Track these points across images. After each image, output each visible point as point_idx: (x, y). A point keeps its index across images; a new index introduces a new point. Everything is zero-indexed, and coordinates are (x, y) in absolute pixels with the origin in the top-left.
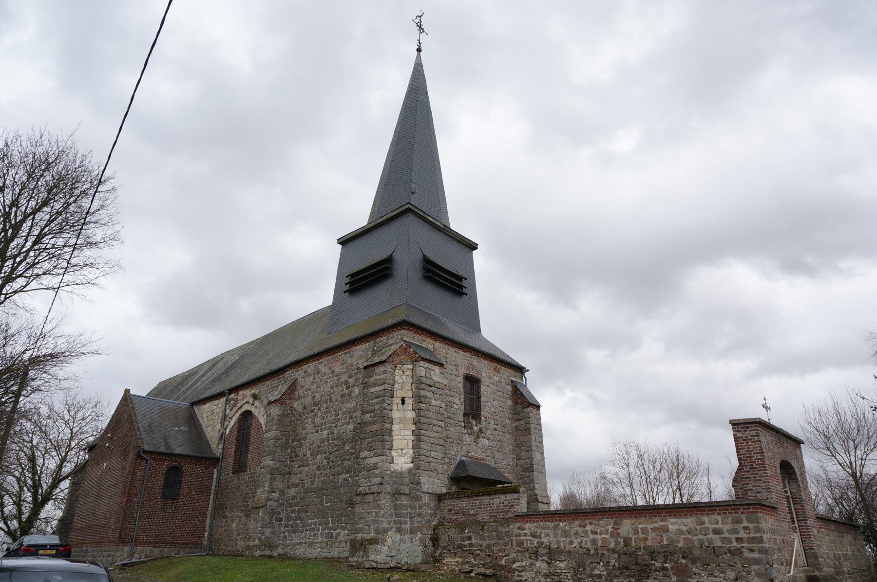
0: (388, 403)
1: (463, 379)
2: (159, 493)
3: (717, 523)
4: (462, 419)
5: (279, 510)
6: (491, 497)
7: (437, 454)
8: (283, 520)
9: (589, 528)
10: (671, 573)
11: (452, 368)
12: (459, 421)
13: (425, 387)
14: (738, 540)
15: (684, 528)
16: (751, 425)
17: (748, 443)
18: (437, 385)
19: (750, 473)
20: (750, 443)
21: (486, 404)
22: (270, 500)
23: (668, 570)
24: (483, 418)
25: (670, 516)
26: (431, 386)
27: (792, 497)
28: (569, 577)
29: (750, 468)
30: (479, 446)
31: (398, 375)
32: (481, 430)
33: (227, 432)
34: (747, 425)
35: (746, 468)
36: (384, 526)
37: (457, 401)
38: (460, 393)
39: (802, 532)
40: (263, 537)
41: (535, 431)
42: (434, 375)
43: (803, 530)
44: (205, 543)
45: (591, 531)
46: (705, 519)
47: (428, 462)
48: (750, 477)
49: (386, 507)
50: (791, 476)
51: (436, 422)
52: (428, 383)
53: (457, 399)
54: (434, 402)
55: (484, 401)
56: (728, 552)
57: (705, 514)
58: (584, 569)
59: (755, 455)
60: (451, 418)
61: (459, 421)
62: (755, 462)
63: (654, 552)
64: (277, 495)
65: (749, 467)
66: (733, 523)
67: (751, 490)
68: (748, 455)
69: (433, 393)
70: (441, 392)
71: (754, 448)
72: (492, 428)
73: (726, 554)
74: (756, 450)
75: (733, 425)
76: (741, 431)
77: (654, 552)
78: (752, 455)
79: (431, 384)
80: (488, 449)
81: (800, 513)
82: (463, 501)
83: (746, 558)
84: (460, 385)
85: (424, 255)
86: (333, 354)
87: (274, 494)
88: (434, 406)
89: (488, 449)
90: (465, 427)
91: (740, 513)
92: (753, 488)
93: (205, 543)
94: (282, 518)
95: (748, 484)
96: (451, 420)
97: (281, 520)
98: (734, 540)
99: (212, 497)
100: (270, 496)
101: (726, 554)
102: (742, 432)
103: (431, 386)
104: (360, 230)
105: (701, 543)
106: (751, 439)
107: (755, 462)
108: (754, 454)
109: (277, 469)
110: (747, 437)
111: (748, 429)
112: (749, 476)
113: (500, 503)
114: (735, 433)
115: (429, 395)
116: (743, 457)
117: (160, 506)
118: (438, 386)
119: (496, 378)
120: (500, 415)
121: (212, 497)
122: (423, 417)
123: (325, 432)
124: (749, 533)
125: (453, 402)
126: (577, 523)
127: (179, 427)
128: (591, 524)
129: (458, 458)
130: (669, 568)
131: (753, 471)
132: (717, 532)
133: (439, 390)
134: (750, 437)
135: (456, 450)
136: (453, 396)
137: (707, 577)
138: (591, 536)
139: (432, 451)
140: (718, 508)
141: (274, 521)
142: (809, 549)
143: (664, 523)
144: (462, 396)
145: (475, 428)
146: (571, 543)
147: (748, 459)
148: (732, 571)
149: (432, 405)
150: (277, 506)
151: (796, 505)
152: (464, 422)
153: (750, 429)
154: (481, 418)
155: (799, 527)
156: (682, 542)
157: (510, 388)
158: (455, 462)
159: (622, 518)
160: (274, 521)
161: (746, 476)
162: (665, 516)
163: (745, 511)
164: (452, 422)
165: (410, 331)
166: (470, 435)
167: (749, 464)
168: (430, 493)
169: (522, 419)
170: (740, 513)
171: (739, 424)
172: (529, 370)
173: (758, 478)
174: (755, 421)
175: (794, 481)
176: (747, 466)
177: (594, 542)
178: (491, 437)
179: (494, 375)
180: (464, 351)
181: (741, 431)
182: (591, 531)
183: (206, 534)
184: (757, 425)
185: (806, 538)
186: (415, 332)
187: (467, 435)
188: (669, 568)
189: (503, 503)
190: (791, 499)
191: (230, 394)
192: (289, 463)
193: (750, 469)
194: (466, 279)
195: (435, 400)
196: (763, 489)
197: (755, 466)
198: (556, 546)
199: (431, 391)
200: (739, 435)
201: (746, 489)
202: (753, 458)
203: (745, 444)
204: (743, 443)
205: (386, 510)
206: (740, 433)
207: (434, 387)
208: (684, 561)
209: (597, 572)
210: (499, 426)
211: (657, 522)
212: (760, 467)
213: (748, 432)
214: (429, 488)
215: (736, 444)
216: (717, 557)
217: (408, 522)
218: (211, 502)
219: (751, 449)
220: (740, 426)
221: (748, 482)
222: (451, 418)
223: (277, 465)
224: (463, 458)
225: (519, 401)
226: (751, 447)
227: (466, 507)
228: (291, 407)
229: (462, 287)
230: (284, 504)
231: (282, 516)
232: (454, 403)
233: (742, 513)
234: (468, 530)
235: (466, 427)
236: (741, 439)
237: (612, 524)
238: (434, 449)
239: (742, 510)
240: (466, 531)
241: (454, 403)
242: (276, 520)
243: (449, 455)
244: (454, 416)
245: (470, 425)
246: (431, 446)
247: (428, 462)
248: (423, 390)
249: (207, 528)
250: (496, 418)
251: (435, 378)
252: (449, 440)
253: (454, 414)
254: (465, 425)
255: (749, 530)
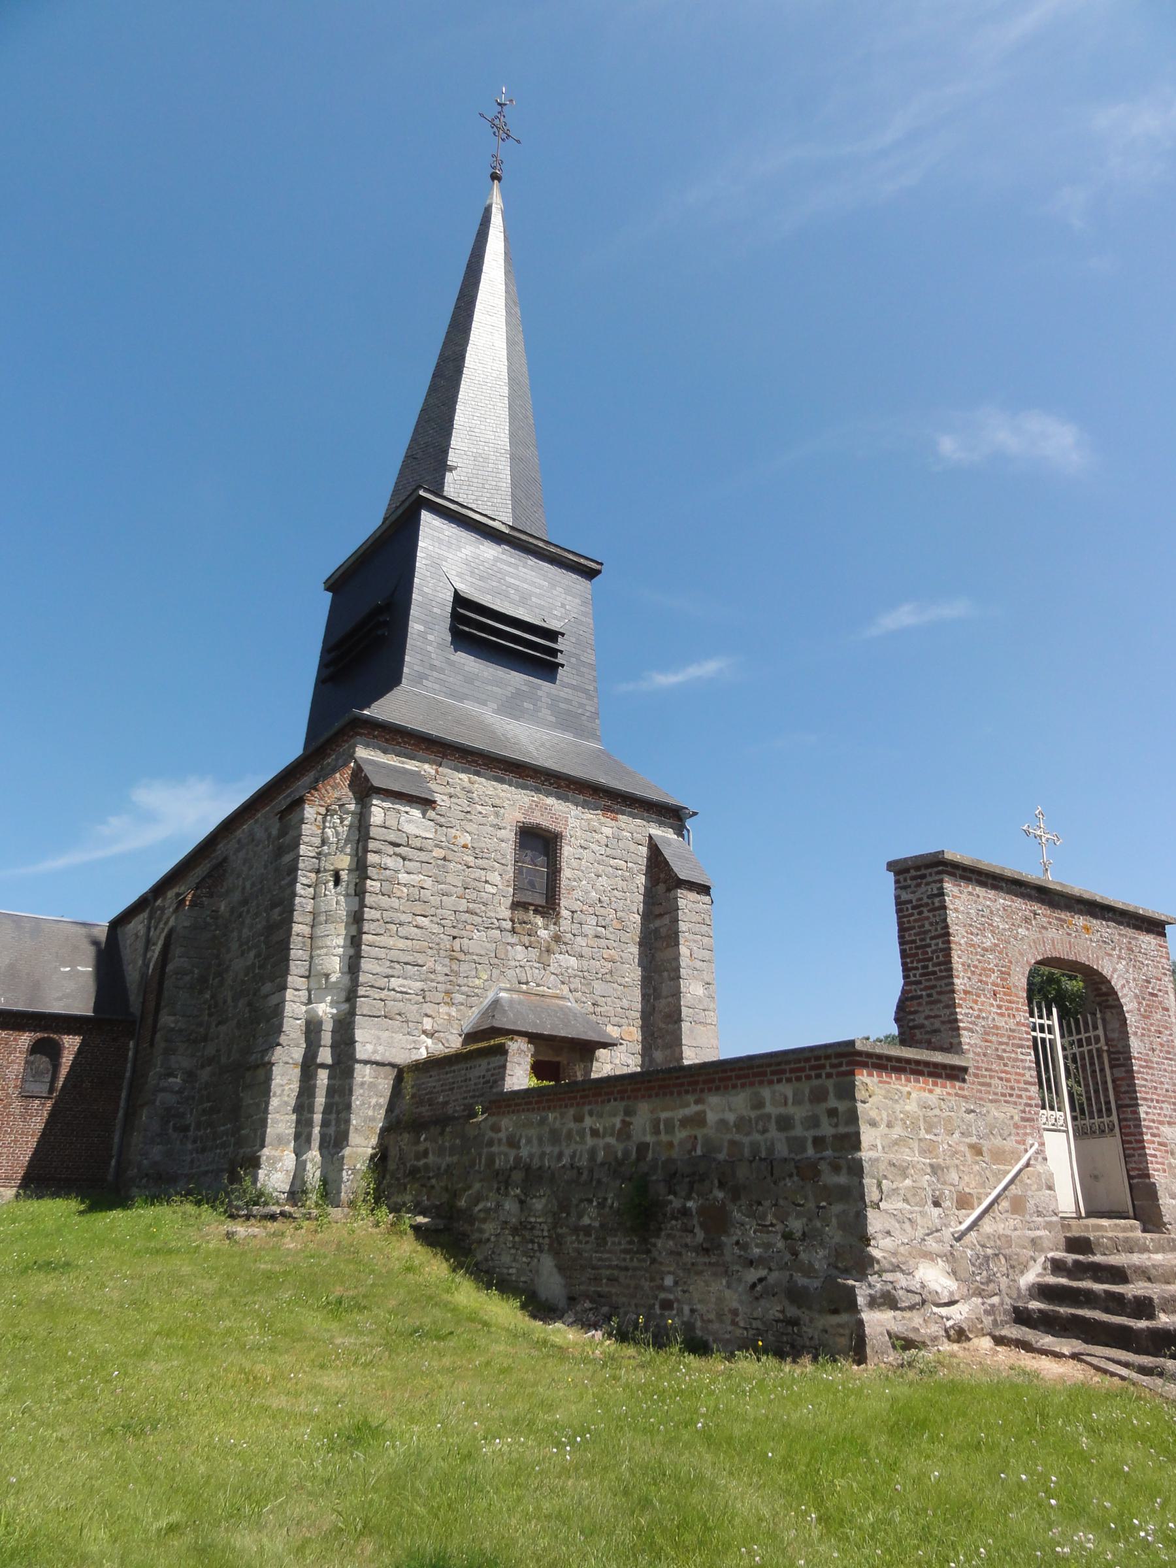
0: (305, 882)
1: (513, 834)
2: (16, 1086)
3: (786, 1104)
4: (507, 914)
5: (181, 1110)
6: (468, 1066)
7: (405, 982)
8: (192, 1128)
9: (588, 1122)
10: (695, 1222)
11: (484, 812)
12: (498, 920)
13: (381, 847)
14: (818, 1142)
15: (731, 1118)
16: (929, 871)
17: (920, 913)
18: (417, 843)
19: (922, 986)
20: (926, 914)
21: (575, 883)
22: (163, 1090)
23: (691, 1215)
24: (565, 913)
25: (710, 1090)
26: (398, 845)
27: (1108, 1051)
28: (546, 1234)
29: (922, 975)
30: (552, 969)
31: (330, 828)
32: (557, 939)
33: (150, 971)
34: (923, 872)
35: (915, 976)
36: (279, 1130)
37: (494, 877)
38: (503, 862)
39: (1127, 1135)
40: (145, 1161)
41: (691, 937)
42: (409, 822)
43: (1127, 1131)
44: (110, 1178)
45: (591, 1129)
46: (766, 1093)
47: (381, 1000)
48: (921, 997)
49: (286, 1093)
50: (1107, 1001)
51: (404, 918)
52: (392, 837)
53: (496, 873)
54: (403, 877)
55: (569, 876)
56: (795, 1172)
57: (766, 1083)
58: (568, 1214)
59: (933, 942)
60: (476, 914)
61: (498, 920)
62: (931, 959)
63: (675, 1173)
64: (178, 1080)
65: (921, 971)
66: (811, 1101)
67: (922, 1026)
68: (919, 943)
69: (404, 859)
70: (423, 856)
71: (931, 924)
72: (591, 933)
73: (791, 1176)
74: (936, 930)
75: (897, 874)
76: (909, 886)
77: (675, 1173)
78: (928, 941)
79: (399, 841)
80: (575, 976)
81: (1123, 1089)
82: (431, 1076)
83: (825, 1186)
84: (503, 844)
85: (456, 591)
86: (271, 801)
87: (171, 1080)
88: (405, 885)
89: (575, 976)
90: (513, 931)
91: (824, 1076)
92: (926, 1022)
93: (110, 1178)
94: (190, 1125)
95: (916, 1012)
96: (475, 917)
97: (186, 1129)
98: (810, 1142)
99: (124, 1095)
100: (163, 1084)
101: (791, 1176)
102: (913, 889)
103: (398, 845)
104: (354, 558)
105: (755, 1148)
106: (927, 904)
107: (931, 959)
108: (932, 938)
109: (181, 1031)
110: (921, 899)
111: (924, 881)
112: (919, 993)
113: (479, 1077)
114: (899, 891)
115: (389, 862)
116: (911, 949)
117: (18, 1111)
118: (419, 845)
119: (608, 831)
120: (614, 906)
121: (124, 1095)
122: (371, 908)
123: (252, 954)
124: (836, 1126)
125: (484, 879)
126: (571, 1112)
127: (73, 967)
128: (591, 1114)
129: (491, 996)
130: (694, 1211)
131: (926, 980)
132: (785, 1123)
133: (419, 853)
134: (926, 900)
135: (485, 977)
136: (484, 869)
137: (754, 1232)
138: (590, 1141)
139: (393, 976)
140: (787, 1067)
141: (170, 1131)
142: (1139, 1176)
143: (699, 1107)
144: (510, 869)
145: (543, 933)
146: (560, 1156)
147: (920, 952)
148: (799, 1216)
149: (398, 884)
150: (178, 1103)
151: (1115, 1070)
152: (512, 920)
153: (929, 879)
154: (559, 913)
155: (1120, 1120)
156: (725, 1151)
157: (644, 850)
158: (481, 1002)
159: (636, 1098)
160: (170, 1131)
161: (914, 994)
162: (702, 1091)
163: (834, 1071)
164: (477, 920)
165: (375, 737)
166: (527, 948)
167: (919, 965)
168: (377, 1063)
169: (665, 914)
170: (824, 1076)
171: (907, 871)
172: (695, 814)
173: (935, 996)
174: (936, 860)
175: (1114, 1011)
176: (916, 968)
177: (593, 1153)
178: (586, 951)
179: (601, 824)
180: (521, 777)
181: (909, 886)
182: (591, 1129)
183: (113, 1163)
184: (941, 868)
185: (1134, 1149)
186: (387, 741)
187: (519, 948)
188: (694, 1211)
189: (484, 1077)
190: (1105, 1055)
191: (155, 900)
192: (206, 1018)
193: (922, 975)
194: (563, 635)
195: (408, 873)
196: (943, 1023)
197: (931, 969)
198: (539, 1164)
199: (399, 855)
200: (905, 896)
201: (911, 1024)
202: (929, 950)
203: (917, 917)
204: (912, 915)
205: (286, 1099)
206: (909, 890)
207: (408, 845)
208: (720, 1195)
209: (586, 1221)
210: (611, 929)
211: (688, 1105)
212: (941, 971)
213: (923, 888)
214: (375, 1052)
215: (899, 918)
216: (775, 1183)
217: (333, 1123)
218: (122, 1104)
219: (927, 927)
220: (908, 876)
221: (916, 1008)
222: (476, 914)
223: (179, 1024)
224: (503, 994)
225: (662, 876)
226: (926, 923)
227: (434, 1087)
228: (213, 911)
229: (554, 652)
230: (193, 1098)
231: (188, 1122)
232: (486, 882)
233: (829, 1076)
234: (424, 1136)
235: (516, 930)
236: (909, 906)
237: (622, 1113)
238: (396, 973)
239: (828, 1070)
240: (422, 1139)
241: (486, 882)
242: (175, 1129)
243: (464, 989)
244: (483, 908)
245: (529, 926)
246: (390, 967)
247: (381, 1000)
248: (375, 852)
249: (115, 1152)
250: (602, 911)
251: (410, 829)
252: (468, 957)
253: (485, 904)
254: (513, 928)
255: (837, 1116)
